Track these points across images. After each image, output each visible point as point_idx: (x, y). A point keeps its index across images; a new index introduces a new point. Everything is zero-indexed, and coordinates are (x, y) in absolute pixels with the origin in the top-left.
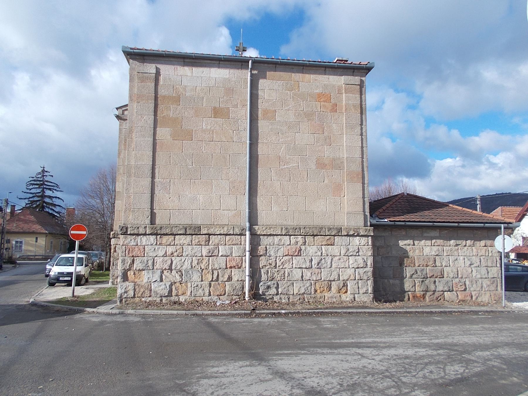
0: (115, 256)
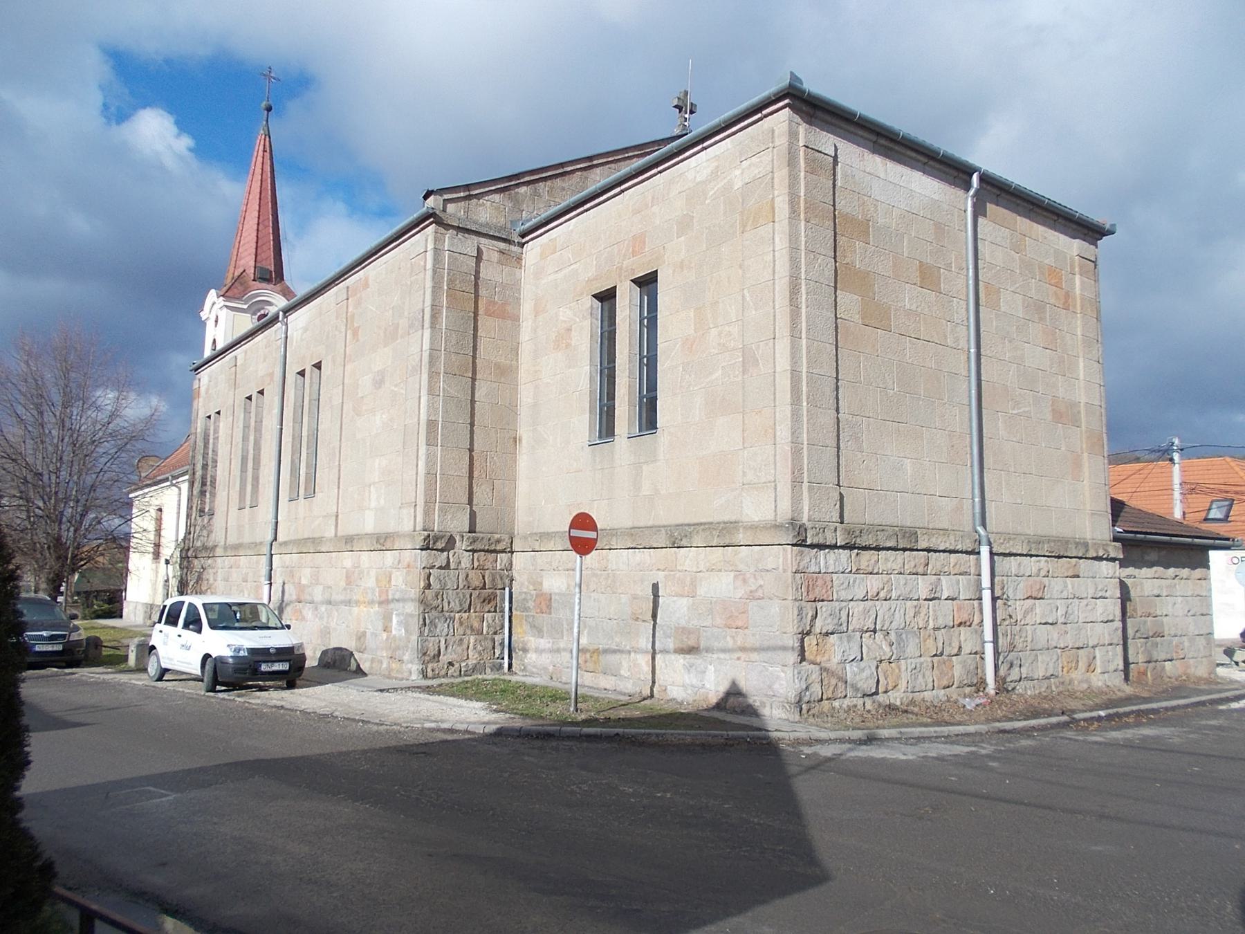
0: (429, 598)
